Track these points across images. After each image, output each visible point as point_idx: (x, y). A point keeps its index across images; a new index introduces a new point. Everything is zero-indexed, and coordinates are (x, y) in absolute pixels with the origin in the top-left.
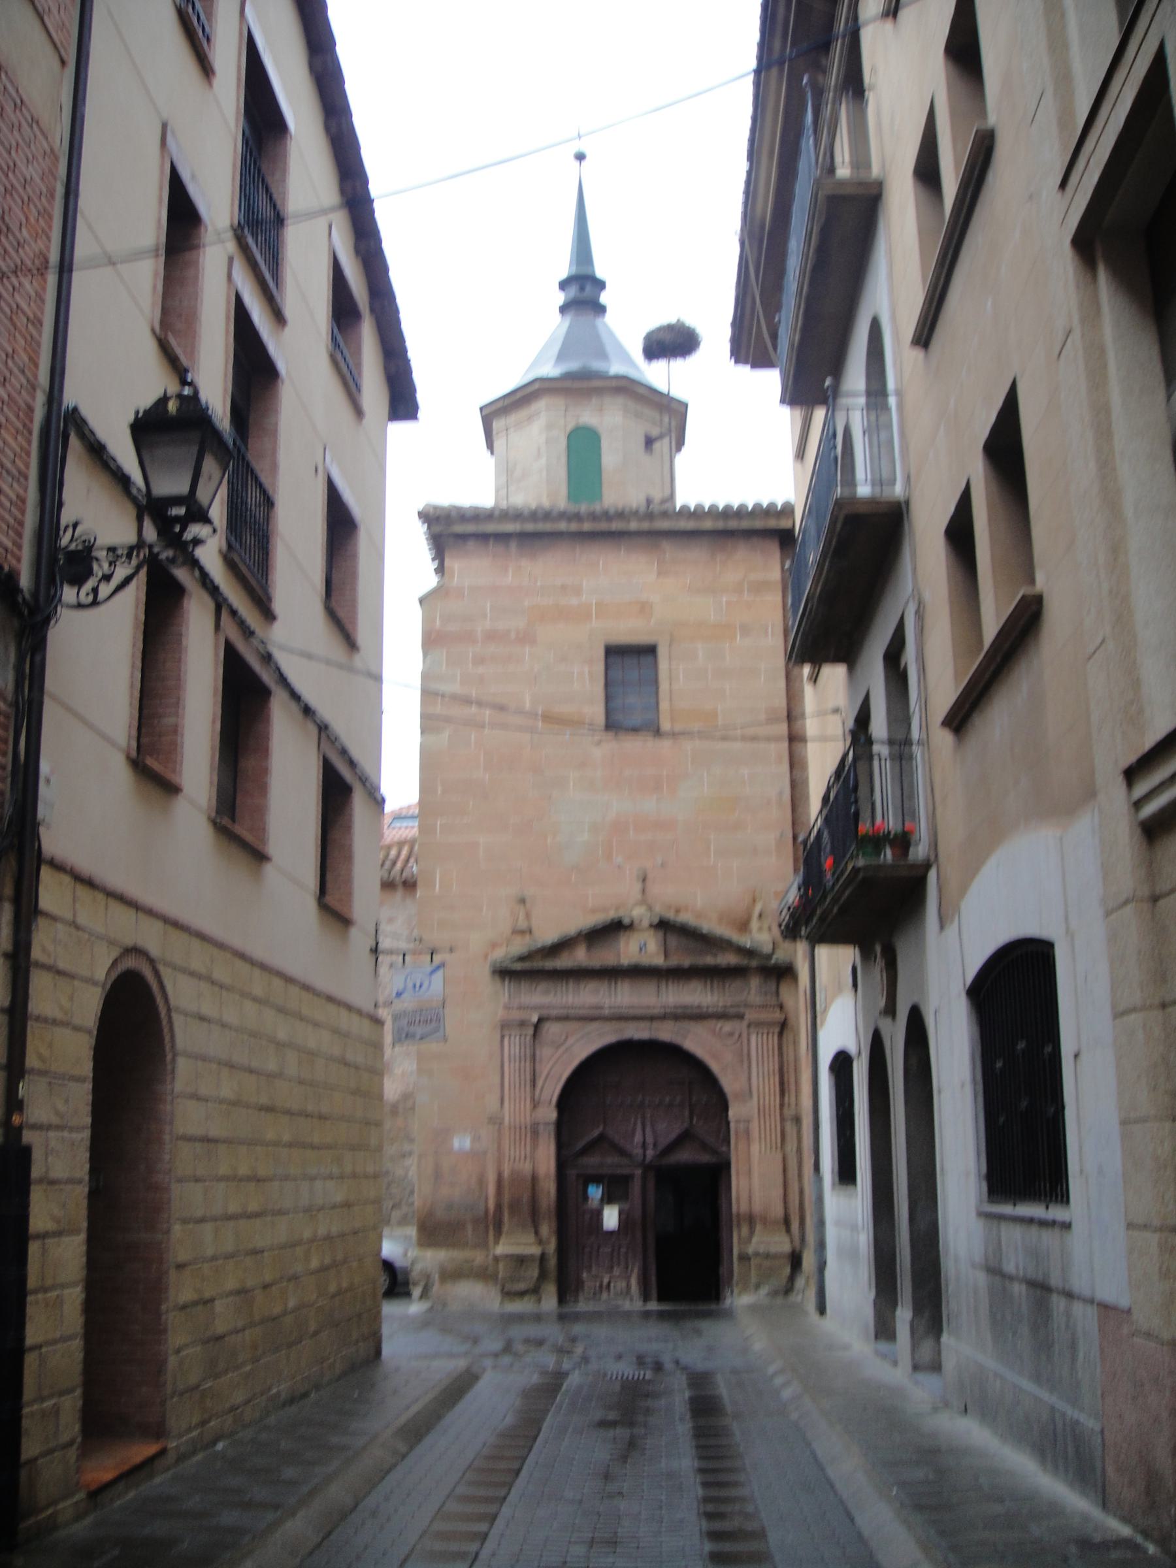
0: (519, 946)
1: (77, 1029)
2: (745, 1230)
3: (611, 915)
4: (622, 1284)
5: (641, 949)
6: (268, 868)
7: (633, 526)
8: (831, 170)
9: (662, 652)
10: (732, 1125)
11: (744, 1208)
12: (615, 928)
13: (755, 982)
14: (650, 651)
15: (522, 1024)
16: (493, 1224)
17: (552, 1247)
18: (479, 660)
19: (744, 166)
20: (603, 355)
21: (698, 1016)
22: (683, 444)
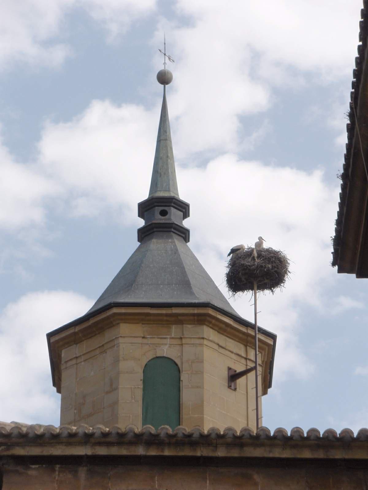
7: (221, 453)
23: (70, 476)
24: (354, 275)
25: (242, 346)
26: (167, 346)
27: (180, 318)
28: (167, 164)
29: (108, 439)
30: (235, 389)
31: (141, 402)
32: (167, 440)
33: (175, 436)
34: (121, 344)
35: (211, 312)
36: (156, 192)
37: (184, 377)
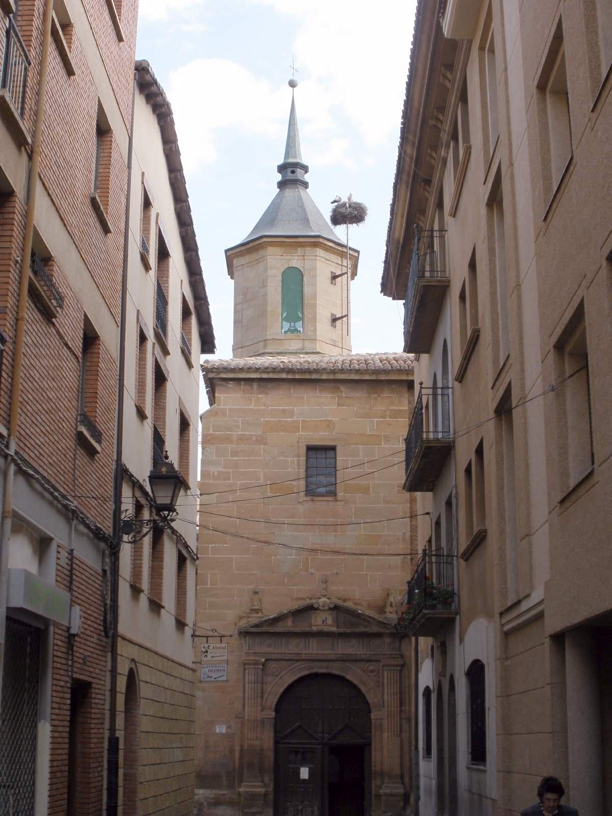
0: (255, 619)
1: (122, 693)
2: (378, 782)
3: (308, 602)
4: (309, 809)
5: (324, 621)
6: (163, 611)
7: (324, 377)
8: (423, 276)
9: (339, 450)
10: (373, 721)
11: (378, 768)
12: (310, 608)
13: (387, 640)
14: (333, 448)
15: (256, 663)
16: (235, 776)
17: (271, 789)
18: (235, 453)
19: (388, 217)
20: (306, 221)
21: (356, 660)
22: (356, 275)
23: (249, 387)
24: (391, 298)
25: (340, 258)
26: (295, 261)
27: (303, 244)
28: (295, 140)
29: (268, 370)
30: (335, 284)
31: (280, 294)
32: (297, 371)
33: (301, 369)
34: (268, 257)
35: (321, 240)
36: (288, 158)
37: (305, 279)
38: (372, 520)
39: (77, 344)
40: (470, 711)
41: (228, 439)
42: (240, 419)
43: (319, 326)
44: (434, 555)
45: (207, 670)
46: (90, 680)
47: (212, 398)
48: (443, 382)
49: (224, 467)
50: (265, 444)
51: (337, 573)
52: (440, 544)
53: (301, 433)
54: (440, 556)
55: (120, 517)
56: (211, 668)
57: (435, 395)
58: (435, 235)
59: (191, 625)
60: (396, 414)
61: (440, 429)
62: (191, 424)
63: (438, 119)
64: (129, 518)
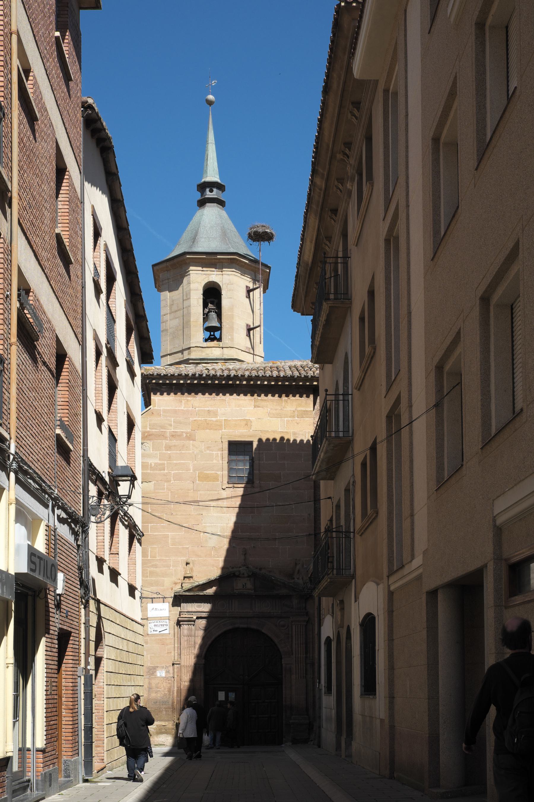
0: (188, 585)
5: (243, 586)
10: (284, 665)
18: (168, 448)
38: (283, 504)
39: (52, 363)
40: (363, 653)
41: (162, 436)
42: (172, 419)
43: (236, 335)
44: (334, 532)
45: (153, 625)
46: (69, 629)
47: (148, 400)
48: (344, 389)
49: (160, 460)
50: (194, 440)
51: (254, 547)
52: (340, 523)
53: (223, 430)
54: (340, 532)
55: (88, 503)
56: (156, 624)
57: (337, 401)
58: (339, 261)
59: (139, 589)
60: (303, 414)
61: (341, 428)
62: (136, 425)
63: (345, 154)
64: (95, 503)
